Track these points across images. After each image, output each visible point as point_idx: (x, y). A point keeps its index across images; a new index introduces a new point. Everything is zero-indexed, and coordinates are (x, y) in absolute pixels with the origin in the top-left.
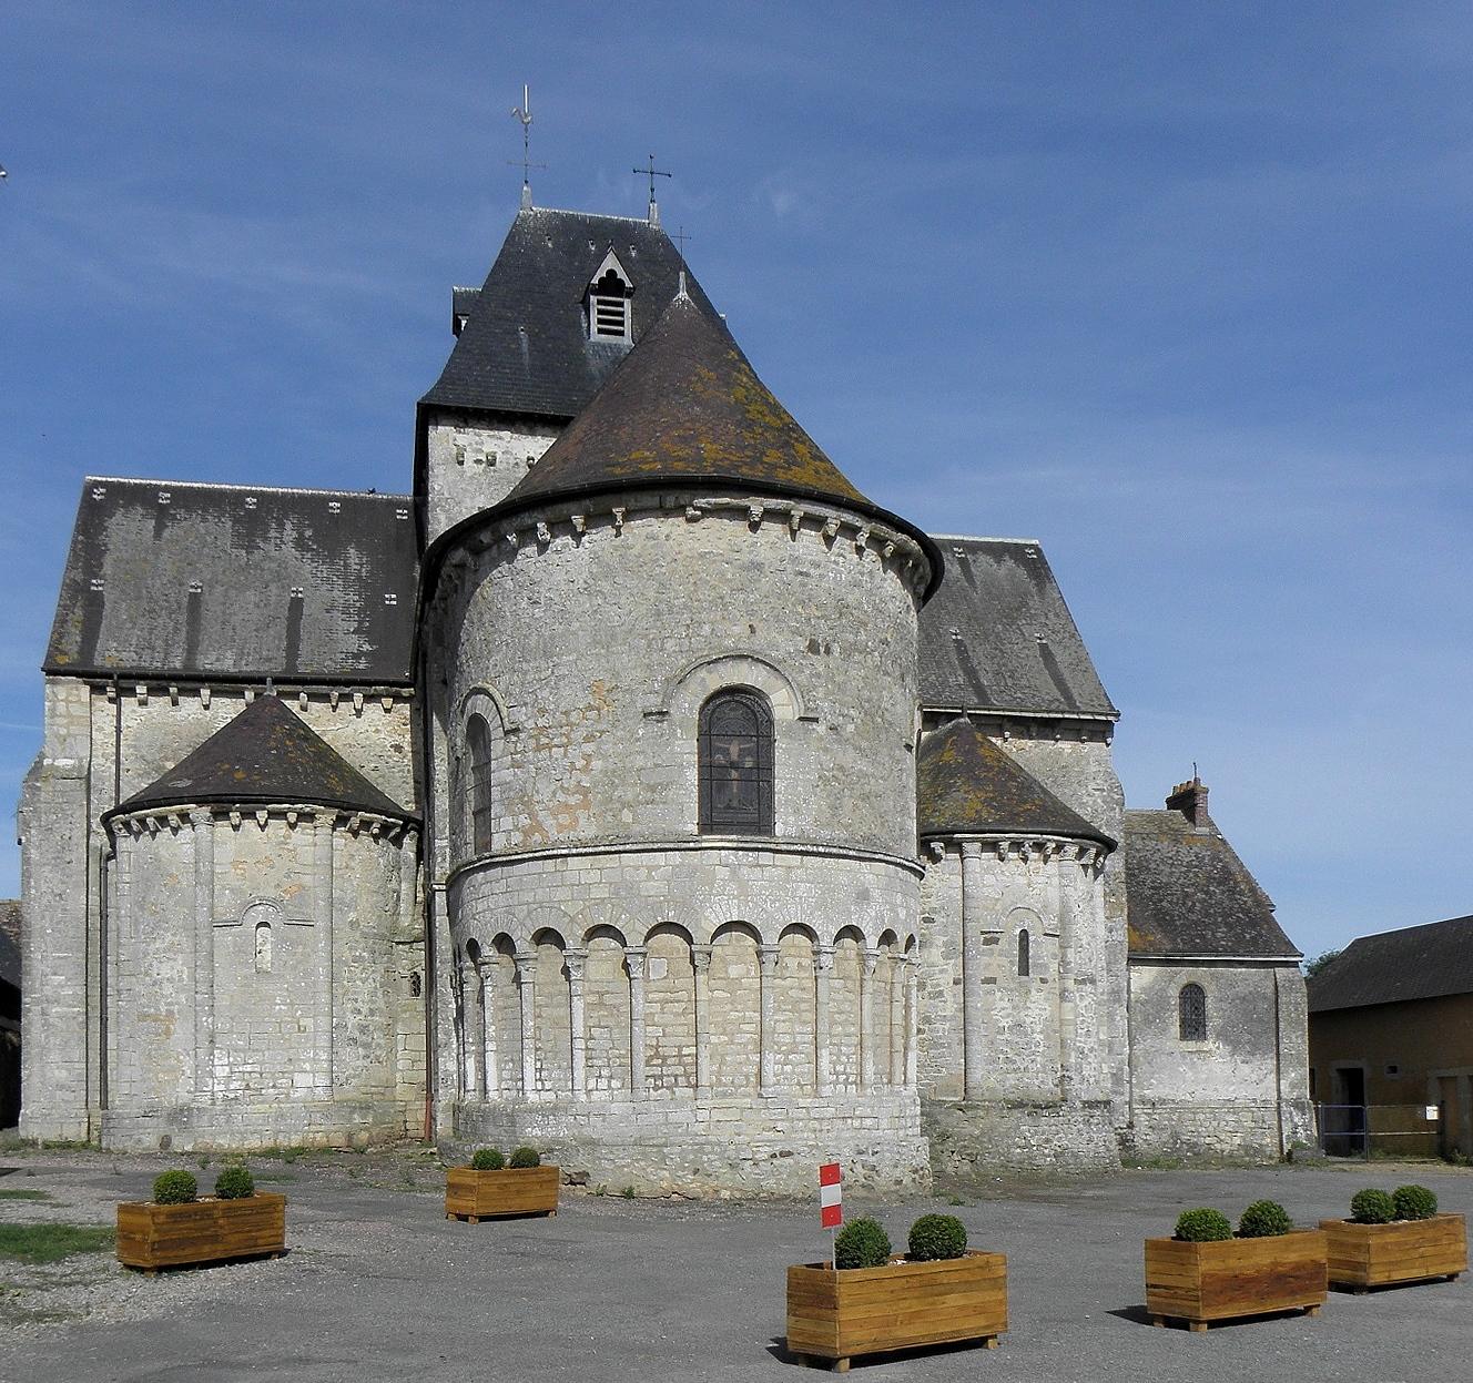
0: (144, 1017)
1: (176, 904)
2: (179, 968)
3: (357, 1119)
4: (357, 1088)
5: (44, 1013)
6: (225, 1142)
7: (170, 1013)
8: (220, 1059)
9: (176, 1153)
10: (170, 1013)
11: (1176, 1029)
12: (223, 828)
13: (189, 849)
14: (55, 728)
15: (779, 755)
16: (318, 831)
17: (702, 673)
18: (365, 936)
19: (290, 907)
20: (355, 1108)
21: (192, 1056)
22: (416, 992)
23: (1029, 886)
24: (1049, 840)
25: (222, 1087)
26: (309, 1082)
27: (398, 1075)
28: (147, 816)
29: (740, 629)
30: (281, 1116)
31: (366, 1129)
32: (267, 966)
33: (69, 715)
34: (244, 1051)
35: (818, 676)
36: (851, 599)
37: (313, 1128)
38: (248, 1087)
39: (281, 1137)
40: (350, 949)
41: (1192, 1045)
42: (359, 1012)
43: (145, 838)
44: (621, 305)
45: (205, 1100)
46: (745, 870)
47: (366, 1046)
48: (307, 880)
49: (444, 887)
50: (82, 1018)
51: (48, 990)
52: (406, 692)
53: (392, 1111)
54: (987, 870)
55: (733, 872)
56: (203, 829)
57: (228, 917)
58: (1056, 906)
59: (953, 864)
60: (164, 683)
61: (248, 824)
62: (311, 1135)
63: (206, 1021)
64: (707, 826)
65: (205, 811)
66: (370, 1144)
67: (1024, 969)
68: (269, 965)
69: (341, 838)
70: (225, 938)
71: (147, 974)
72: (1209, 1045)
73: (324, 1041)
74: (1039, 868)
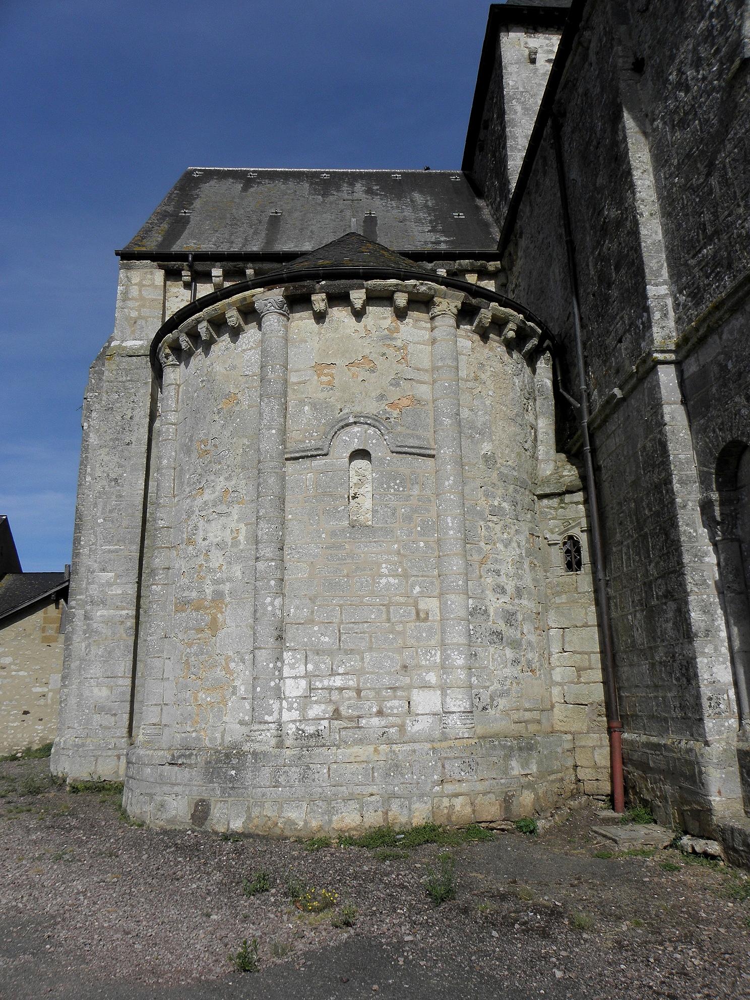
0: (183, 604)
1: (232, 435)
2: (233, 525)
3: (516, 768)
4: (506, 713)
5: (87, 617)
6: (299, 817)
7: (218, 596)
8: (292, 667)
9: (216, 833)
10: (218, 596)
12: (303, 321)
13: (254, 356)
14: (126, 310)
16: (438, 322)
18: (504, 478)
19: (399, 429)
20: (511, 748)
21: (248, 663)
22: (573, 564)
25: (295, 715)
26: (434, 706)
27: (556, 691)
28: (198, 321)
30: (395, 767)
31: (530, 786)
32: (366, 518)
33: (141, 298)
34: (330, 653)
37: (449, 788)
38: (337, 715)
39: (395, 806)
40: (487, 495)
42: (503, 591)
43: (198, 360)
45: (266, 738)
47: (515, 644)
48: (424, 391)
49: (672, 357)
50: (131, 623)
51: (94, 590)
52: (492, 266)
53: (559, 750)
56: (272, 321)
57: (308, 444)
60: (240, 264)
61: (339, 314)
62: (446, 802)
63: (271, 603)
65: (277, 294)
66: (538, 812)
68: (369, 516)
69: (467, 339)
70: (303, 475)
71: (190, 542)
73: (457, 636)
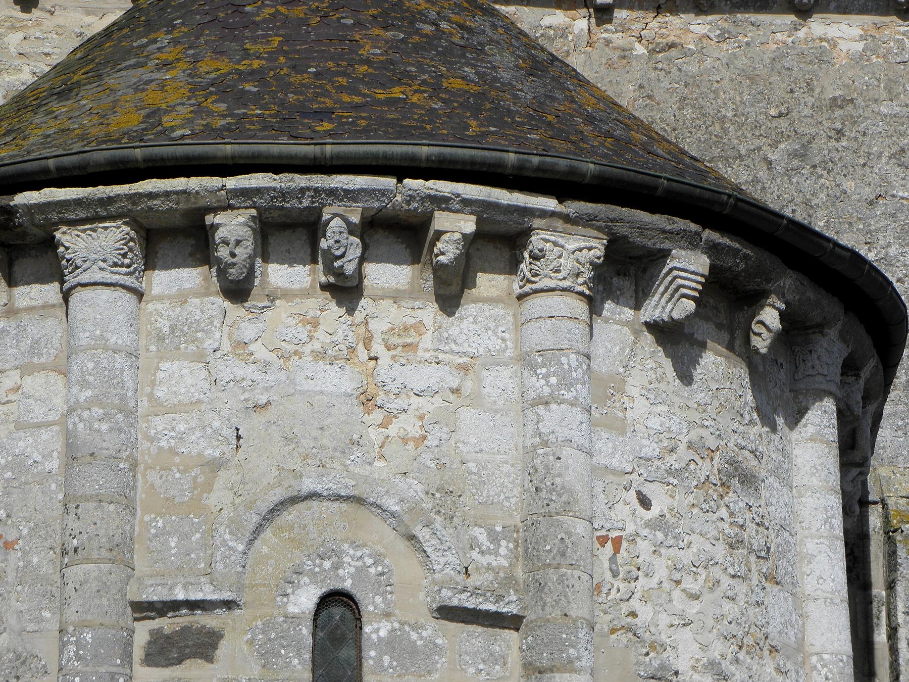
23: (367, 401)
24: (442, 202)
54: (177, 340)
58: (506, 491)
59: (36, 328)
74: (419, 327)
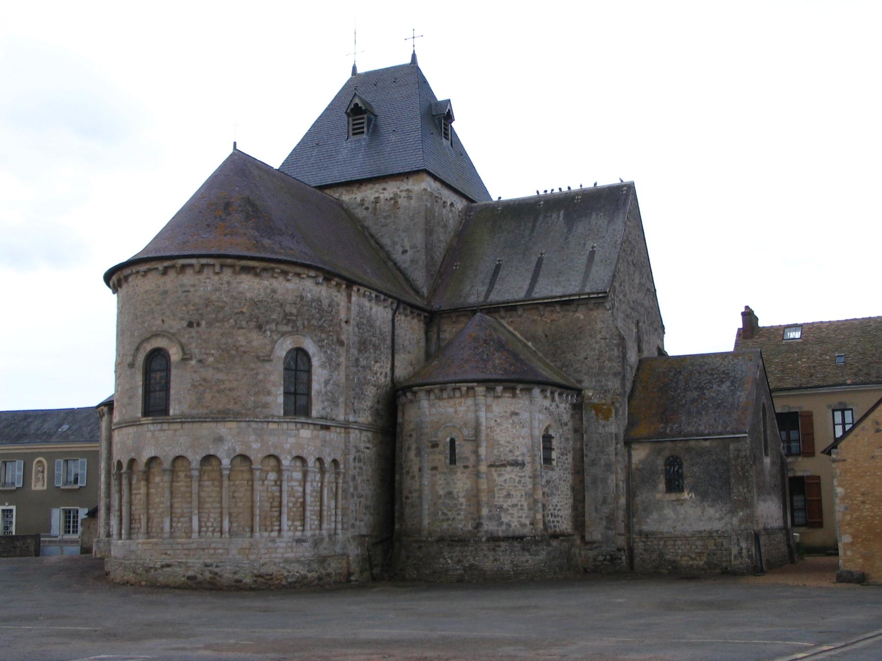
11: (662, 486)
15: (173, 378)
17: (145, 345)
29: (159, 322)
35: (192, 337)
36: (214, 297)
41: (673, 496)
44: (363, 118)
46: (157, 433)
55: (153, 434)
64: (146, 413)
67: (453, 461)
72: (686, 495)
